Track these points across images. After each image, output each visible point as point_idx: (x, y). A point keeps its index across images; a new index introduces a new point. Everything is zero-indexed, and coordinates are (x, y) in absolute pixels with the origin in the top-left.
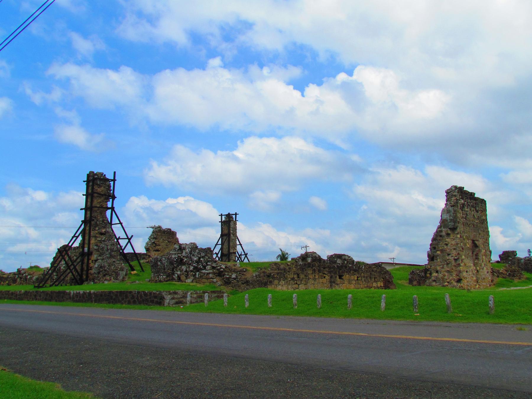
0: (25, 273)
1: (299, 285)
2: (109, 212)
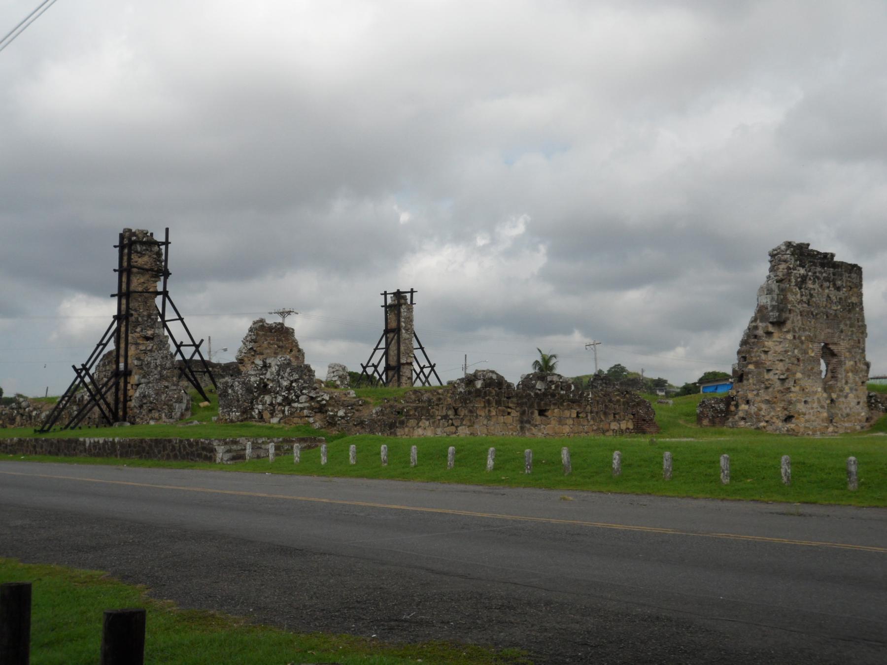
0: (28, 406)
1: (457, 427)
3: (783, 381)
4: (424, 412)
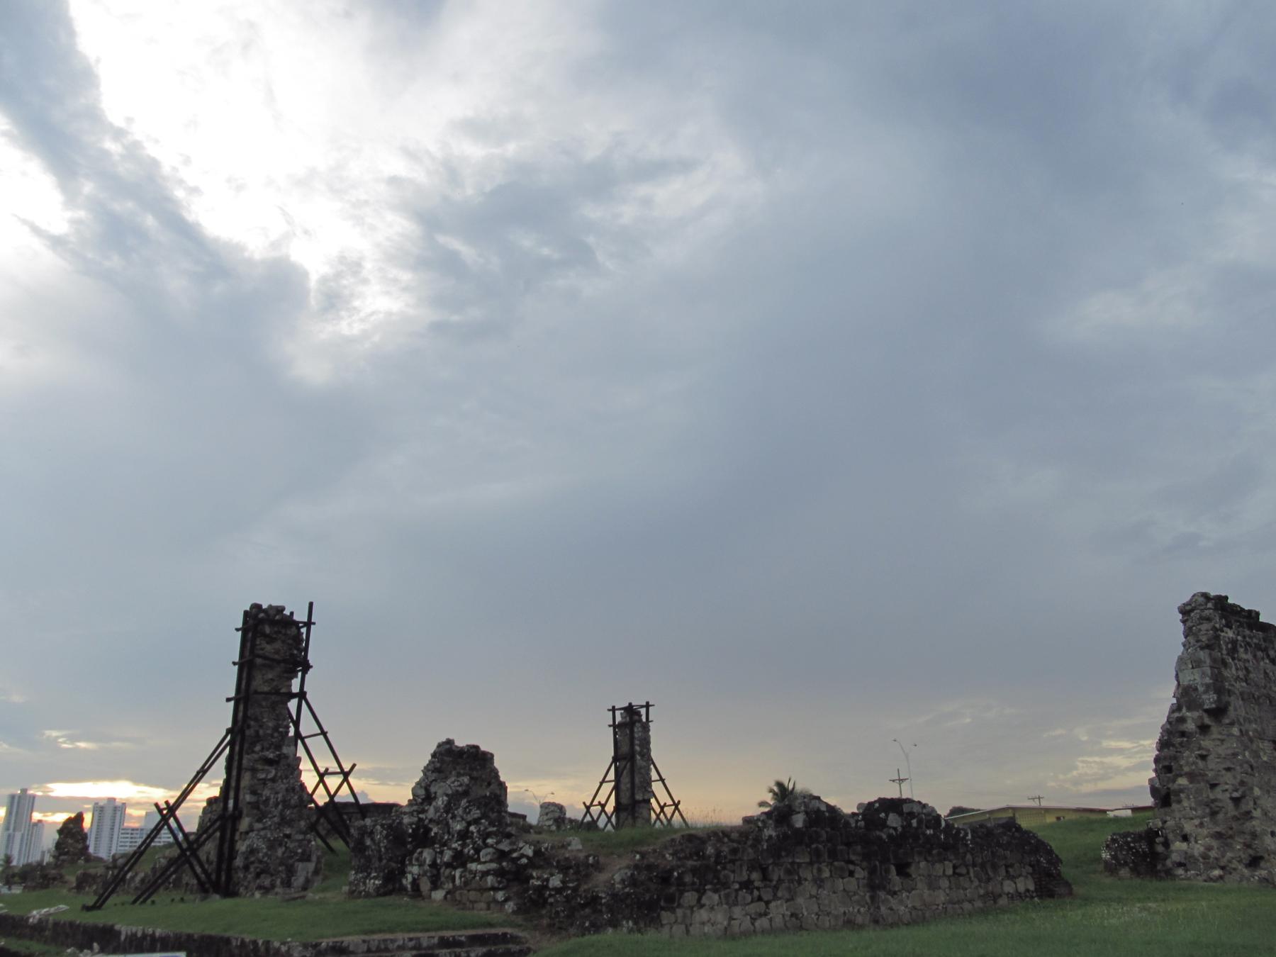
1: (767, 903)
2: (292, 705)
3: (1237, 801)
4: (710, 876)
